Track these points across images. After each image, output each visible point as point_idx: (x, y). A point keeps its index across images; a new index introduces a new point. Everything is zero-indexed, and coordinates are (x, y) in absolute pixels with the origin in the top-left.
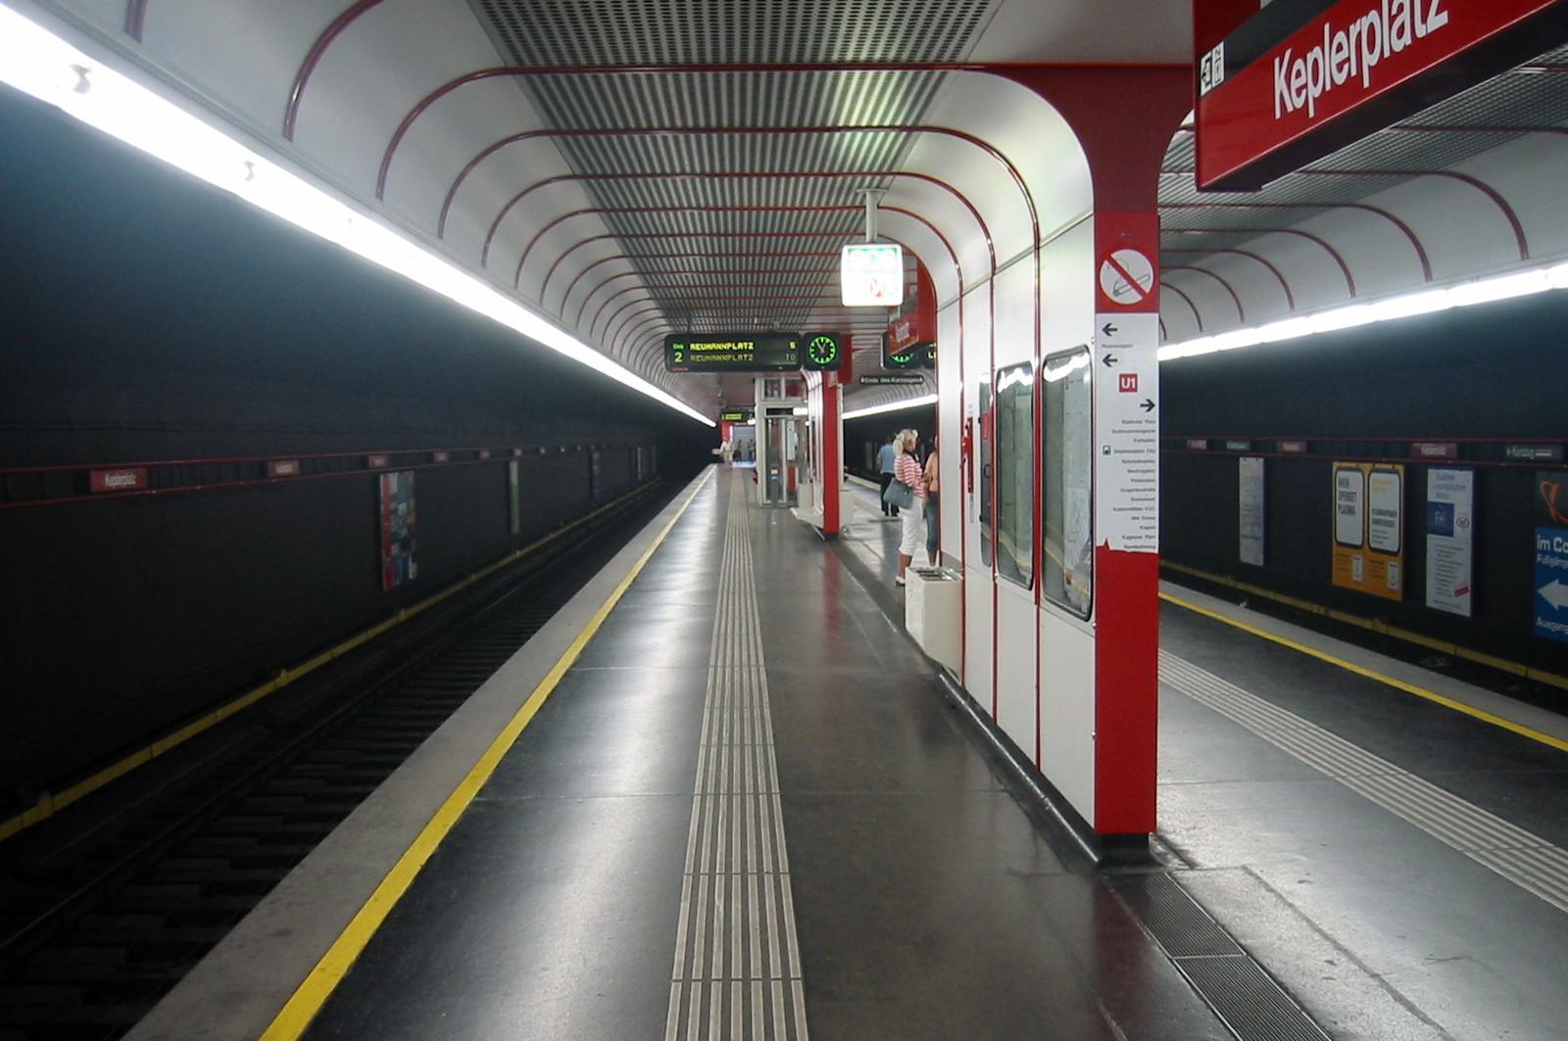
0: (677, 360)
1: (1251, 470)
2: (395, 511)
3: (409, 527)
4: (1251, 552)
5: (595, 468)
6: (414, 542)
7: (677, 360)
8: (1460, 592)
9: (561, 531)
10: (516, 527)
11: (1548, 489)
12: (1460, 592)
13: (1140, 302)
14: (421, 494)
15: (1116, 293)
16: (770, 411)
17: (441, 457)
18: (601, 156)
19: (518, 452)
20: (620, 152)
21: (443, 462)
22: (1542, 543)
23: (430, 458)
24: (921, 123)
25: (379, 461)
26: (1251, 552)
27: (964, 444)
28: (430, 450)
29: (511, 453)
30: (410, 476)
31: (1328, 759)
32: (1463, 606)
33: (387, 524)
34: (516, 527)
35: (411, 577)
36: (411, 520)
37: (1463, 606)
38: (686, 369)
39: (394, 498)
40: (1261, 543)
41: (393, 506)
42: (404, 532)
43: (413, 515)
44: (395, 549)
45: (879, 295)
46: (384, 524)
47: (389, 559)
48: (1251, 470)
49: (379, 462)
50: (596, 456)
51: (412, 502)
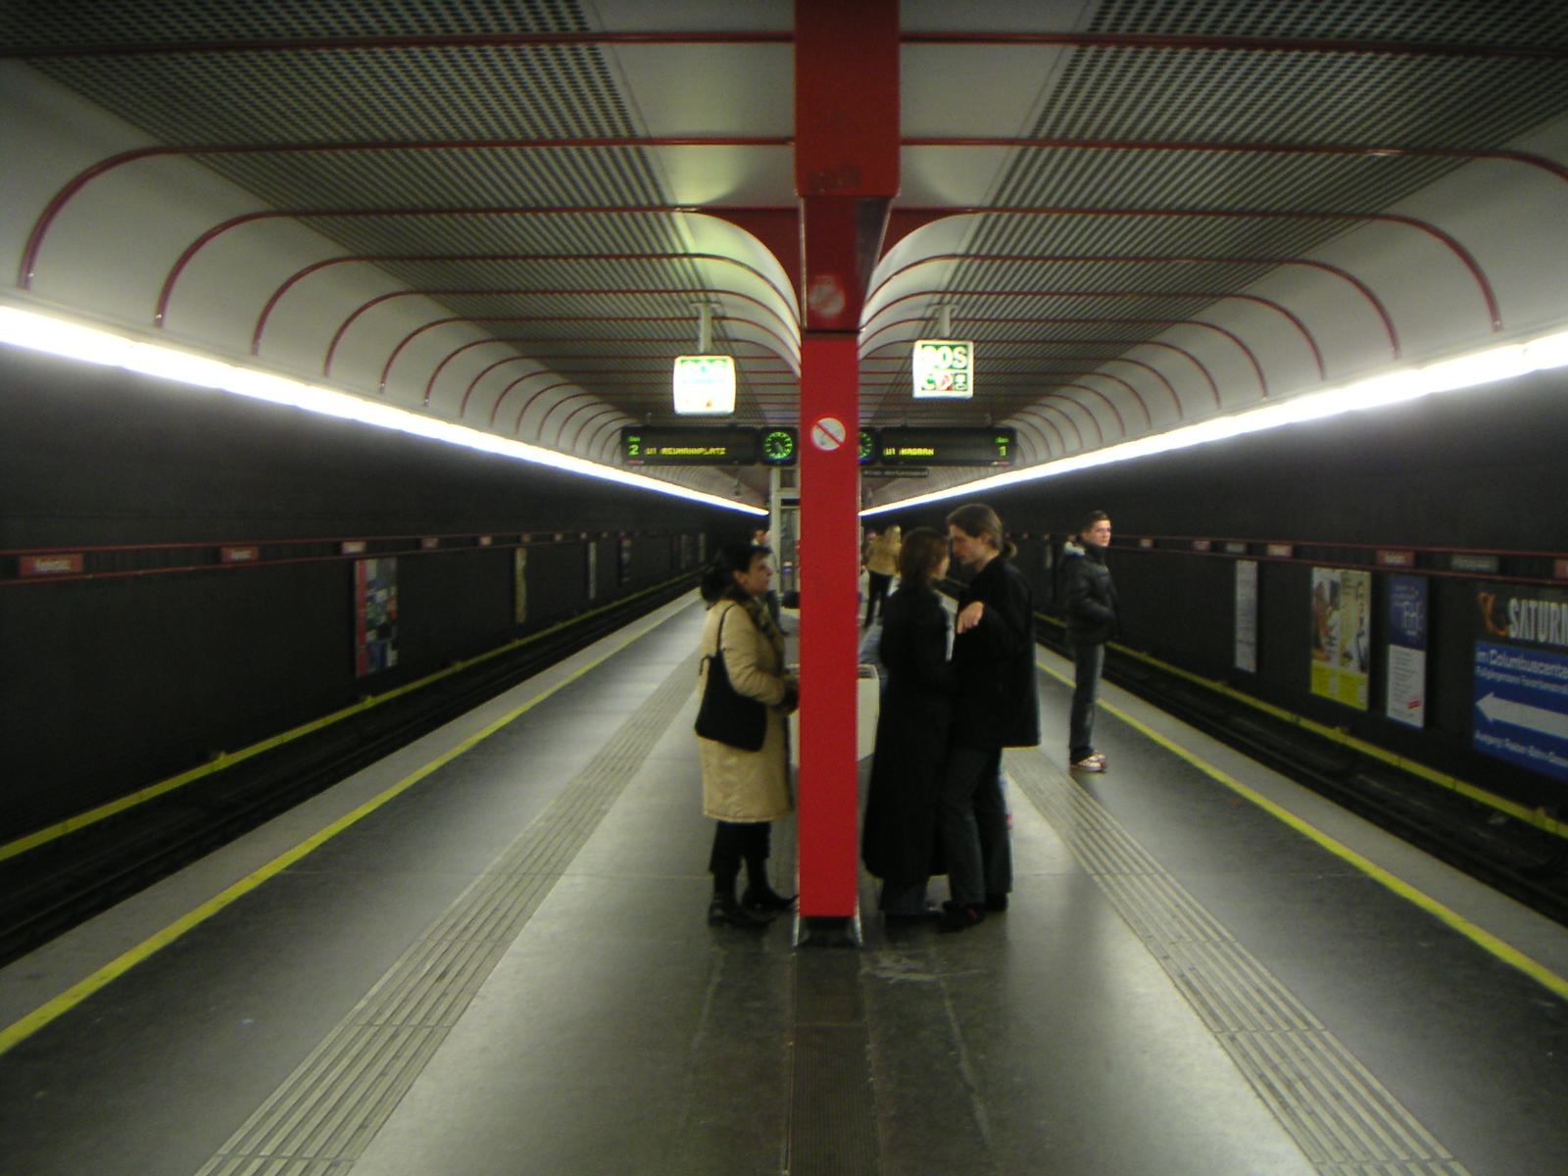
0: (633, 453)
1: (1246, 573)
2: (372, 598)
3: (389, 615)
4: (1245, 659)
5: (626, 556)
6: (394, 630)
7: (633, 453)
8: (1413, 705)
9: (574, 621)
10: (592, 594)
11: (1485, 600)
12: (1413, 705)
13: (835, 450)
14: (404, 581)
15: (823, 444)
16: (785, 502)
17: (430, 543)
18: (424, 81)
19: (526, 538)
20: (484, 92)
21: (485, 536)
22: (1481, 655)
23: (418, 544)
24: (1016, 150)
25: (584, 536)
26: (1245, 659)
27: (759, 906)
28: (418, 537)
29: (518, 540)
30: (392, 564)
31: (1029, 306)
32: (1416, 718)
33: (363, 610)
34: (592, 594)
35: (390, 664)
36: (392, 607)
37: (1416, 718)
38: (642, 462)
39: (370, 585)
40: (1253, 648)
41: (369, 593)
42: (383, 619)
43: (394, 602)
44: (371, 636)
45: (949, 389)
46: (360, 612)
47: (363, 646)
48: (1246, 573)
49: (353, 547)
50: (626, 543)
51: (394, 591)
